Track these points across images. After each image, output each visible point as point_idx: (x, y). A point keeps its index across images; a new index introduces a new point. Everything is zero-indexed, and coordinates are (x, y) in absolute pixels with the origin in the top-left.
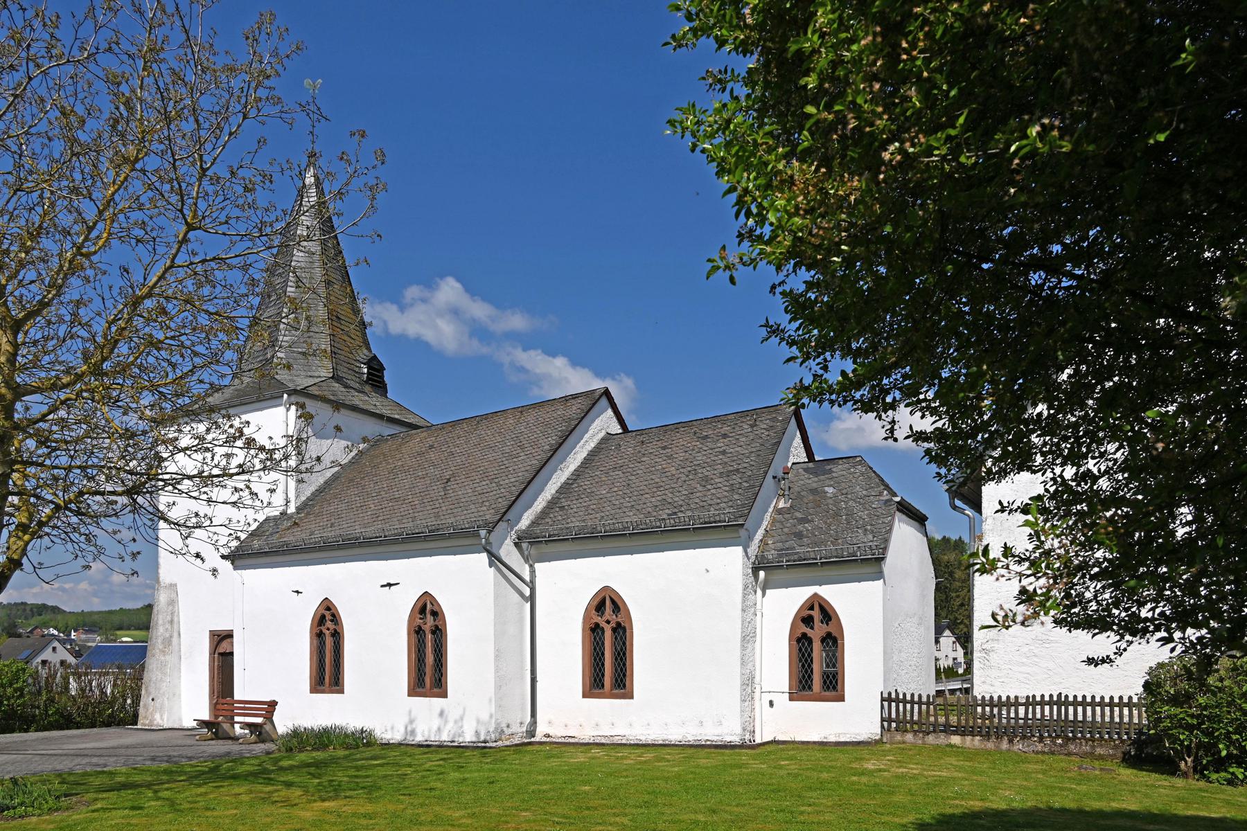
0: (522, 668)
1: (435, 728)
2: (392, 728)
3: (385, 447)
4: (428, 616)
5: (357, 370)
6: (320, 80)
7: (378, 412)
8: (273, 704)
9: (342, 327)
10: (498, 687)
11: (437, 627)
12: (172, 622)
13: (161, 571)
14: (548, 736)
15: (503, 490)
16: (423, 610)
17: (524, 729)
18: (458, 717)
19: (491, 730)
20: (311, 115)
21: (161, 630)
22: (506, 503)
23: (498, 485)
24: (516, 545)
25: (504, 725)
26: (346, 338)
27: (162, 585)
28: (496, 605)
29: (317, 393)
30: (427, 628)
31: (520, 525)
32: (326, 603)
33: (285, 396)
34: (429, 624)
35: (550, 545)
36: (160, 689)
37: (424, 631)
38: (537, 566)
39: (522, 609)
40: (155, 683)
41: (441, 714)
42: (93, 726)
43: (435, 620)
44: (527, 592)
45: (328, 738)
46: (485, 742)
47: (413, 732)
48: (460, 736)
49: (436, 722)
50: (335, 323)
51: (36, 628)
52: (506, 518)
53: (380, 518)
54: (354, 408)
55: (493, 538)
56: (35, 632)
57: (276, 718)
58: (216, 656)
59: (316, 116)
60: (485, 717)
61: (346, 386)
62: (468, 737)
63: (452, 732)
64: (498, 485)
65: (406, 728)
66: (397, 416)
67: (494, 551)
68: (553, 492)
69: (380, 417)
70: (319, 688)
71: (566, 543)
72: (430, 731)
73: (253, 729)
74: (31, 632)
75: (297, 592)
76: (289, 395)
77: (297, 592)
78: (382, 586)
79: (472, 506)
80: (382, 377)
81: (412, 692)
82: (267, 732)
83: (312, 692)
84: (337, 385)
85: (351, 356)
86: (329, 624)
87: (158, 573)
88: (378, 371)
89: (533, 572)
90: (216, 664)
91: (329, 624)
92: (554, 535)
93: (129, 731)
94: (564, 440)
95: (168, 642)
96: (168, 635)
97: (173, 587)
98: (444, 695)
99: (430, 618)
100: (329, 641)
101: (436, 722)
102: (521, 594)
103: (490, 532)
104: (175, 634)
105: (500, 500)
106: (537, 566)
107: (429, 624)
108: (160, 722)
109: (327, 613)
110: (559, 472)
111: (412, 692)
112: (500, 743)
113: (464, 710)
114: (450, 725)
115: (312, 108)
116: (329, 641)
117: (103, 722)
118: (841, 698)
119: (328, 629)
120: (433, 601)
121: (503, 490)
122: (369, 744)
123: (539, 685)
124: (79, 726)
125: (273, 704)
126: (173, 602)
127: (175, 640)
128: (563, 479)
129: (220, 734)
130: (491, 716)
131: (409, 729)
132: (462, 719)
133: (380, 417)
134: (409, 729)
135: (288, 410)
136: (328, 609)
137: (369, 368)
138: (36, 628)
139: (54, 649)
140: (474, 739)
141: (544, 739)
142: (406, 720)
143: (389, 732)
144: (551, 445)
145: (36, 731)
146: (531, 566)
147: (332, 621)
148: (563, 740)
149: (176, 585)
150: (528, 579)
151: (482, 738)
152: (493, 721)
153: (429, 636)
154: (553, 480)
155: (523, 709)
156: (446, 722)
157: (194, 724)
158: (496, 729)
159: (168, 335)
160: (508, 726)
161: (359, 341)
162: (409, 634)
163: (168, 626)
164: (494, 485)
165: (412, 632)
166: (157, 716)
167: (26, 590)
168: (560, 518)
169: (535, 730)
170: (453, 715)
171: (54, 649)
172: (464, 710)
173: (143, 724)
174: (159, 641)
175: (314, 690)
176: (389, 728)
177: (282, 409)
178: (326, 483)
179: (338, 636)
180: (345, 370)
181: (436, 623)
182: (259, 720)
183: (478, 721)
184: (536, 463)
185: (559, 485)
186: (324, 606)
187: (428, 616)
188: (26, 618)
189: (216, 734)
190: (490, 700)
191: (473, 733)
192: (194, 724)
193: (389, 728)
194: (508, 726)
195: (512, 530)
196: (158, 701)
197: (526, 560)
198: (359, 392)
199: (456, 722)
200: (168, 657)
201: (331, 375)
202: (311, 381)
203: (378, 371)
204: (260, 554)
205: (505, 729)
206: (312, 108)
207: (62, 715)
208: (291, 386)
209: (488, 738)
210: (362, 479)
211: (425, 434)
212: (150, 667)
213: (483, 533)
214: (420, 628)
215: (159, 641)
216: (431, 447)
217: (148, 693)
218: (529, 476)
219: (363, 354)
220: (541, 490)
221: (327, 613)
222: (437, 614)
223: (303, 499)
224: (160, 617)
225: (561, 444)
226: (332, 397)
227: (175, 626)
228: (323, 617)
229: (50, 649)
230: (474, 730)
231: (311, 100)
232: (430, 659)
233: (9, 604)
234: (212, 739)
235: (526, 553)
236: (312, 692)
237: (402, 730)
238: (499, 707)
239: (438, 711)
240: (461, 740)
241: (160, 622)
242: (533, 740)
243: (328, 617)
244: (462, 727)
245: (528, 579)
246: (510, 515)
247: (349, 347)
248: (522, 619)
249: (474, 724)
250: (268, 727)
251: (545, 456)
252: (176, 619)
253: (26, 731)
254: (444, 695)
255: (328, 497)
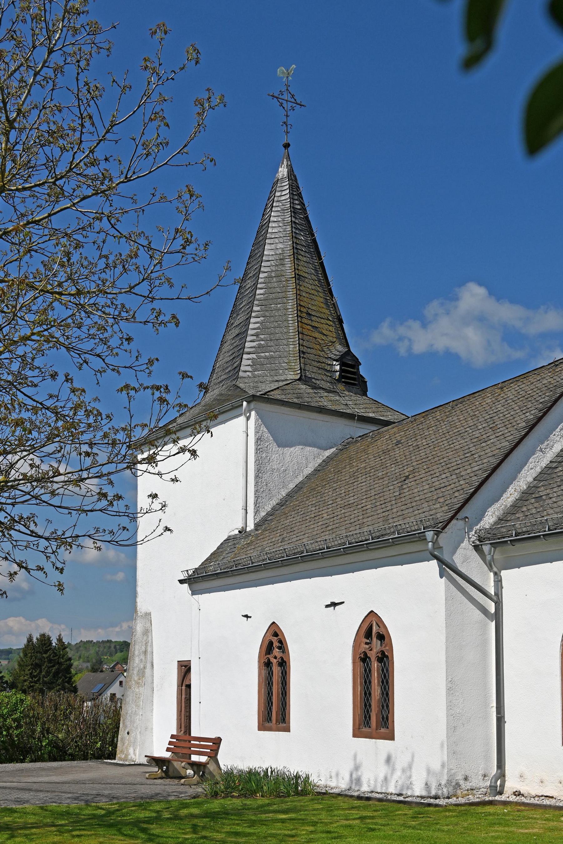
0: (486, 705)
1: (381, 777)
2: (337, 775)
3: (352, 449)
4: (374, 639)
5: (328, 368)
6: (294, 66)
7: (348, 411)
8: (217, 742)
9: (314, 324)
10: (452, 729)
11: (383, 653)
12: (145, 652)
13: (139, 600)
14: (518, 794)
15: (462, 482)
16: (368, 634)
17: (488, 784)
18: (406, 765)
19: (443, 782)
20: (285, 105)
21: (137, 660)
22: (462, 497)
23: (459, 476)
24: (477, 548)
25: (459, 777)
26: (317, 335)
27: (139, 614)
28: (448, 626)
29: (279, 397)
30: (373, 655)
31: (482, 523)
32: (273, 628)
33: (245, 403)
34: (375, 650)
35: (518, 545)
36: (134, 722)
37: (369, 658)
38: (504, 573)
39: (485, 628)
40: (131, 716)
41: (388, 760)
42: (85, 758)
43: (381, 645)
44: (492, 607)
45: (258, 782)
46: (436, 797)
47: (358, 781)
48: (408, 788)
49: (383, 770)
50: (304, 321)
51: (117, 663)
52: (461, 515)
53: (330, 528)
54: (321, 410)
55: (443, 539)
56: (117, 668)
57: (220, 757)
58: (184, 688)
59: (290, 104)
60: (436, 766)
61: (315, 387)
62: (418, 790)
63: (400, 783)
64: (459, 476)
65: (351, 775)
66: (371, 415)
67: (446, 557)
68: (530, 479)
69: (351, 417)
70: (267, 725)
71: (537, 542)
72: (376, 781)
73: (195, 768)
74: (114, 667)
75: (247, 616)
76: (249, 402)
77: (247, 616)
78: (327, 606)
79: (425, 505)
80: (357, 373)
81: (357, 734)
82: (211, 773)
83: (260, 729)
84: (304, 387)
85: (321, 354)
86: (276, 652)
87: (135, 602)
88: (352, 366)
89: (498, 582)
90: (183, 696)
91: (276, 652)
92: (524, 533)
93: (105, 765)
94: (545, 414)
95: (142, 673)
96: (142, 666)
97: (148, 615)
98: (391, 737)
99: (375, 642)
100: (276, 669)
101: (383, 770)
102: (484, 611)
103: (437, 533)
104: (149, 666)
105: (457, 494)
106: (504, 573)
107: (375, 650)
108: (133, 757)
109: (275, 639)
110: (539, 454)
111: (357, 734)
112: (453, 800)
113: (413, 757)
114: (398, 773)
115: (286, 96)
116: (276, 669)
117: (93, 755)
118: (288, 730)
119: (275, 658)
120: (380, 622)
121: (462, 482)
122: (304, 793)
123: (508, 728)
124: (73, 758)
125: (217, 742)
126: (147, 632)
127: (148, 671)
128: (544, 462)
129: (171, 773)
130: (443, 766)
131: (354, 776)
132: (410, 767)
133: (351, 417)
134: (354, 776)
135: (248, 418)
136: (276, 635)
137: (342, 364)
138: (117, 663)
139: (121, 683)
140: (424, 793)
141: (513, 798)
142: (350, 766)
143: (334, 779)
144: (527, 421)
145: (31, 762)
146: (495, 574)
147: (280, 648)
148: (536, 801)
149: (150, 614)
150: (492, 591)
151: (433, 793)
152: (446, 771)
153: (375, 665)
154: (530, 464)
155: (487, 758)
156: (393, 770)
157: (144, 761)
158: (449, 782)
159: (35, 331)
160: (466, 779)
161: (332, 336)
162: (354, 662)
163: (142, 657)
164: (454, 477)
165: (358, 660)
166: (131, 751)
167: (111, 629)
168: (534, 511)
169: (503, 785)
170: (401, 762)
171: (121, 683)
172: (413, 757)
173: (120, 759)
174: (135, 672)
175: (262, 727)
176: (333, 774)
177: (242, 419)
178: (288, 495)
179: (284, 664)
180: (315, 370)
181: (383, 649)
182: (203, 759)
183: (429, 771)
184: (506, 445)
185: (538, 470)
186: (271, 631)
187: (374, 639)
188: (111, 655)
189: (166, 772)
190: (442, 746)
191: (423, 785)
192: (144, 761)
193: (333, 774)
194: (466, 779)
195: (471, 529)
196: (132, 734)
197: (491, 569)
198: (329, 391)
199: (404, 771)
200: (141, 689)
201: (298, 377)
202: (274, 386)
203: (352, 366)
204: (217, 576)
205: (462, 782)
206: (286, 96)
207: (57, 747)
208: (251, 392)
209: (440, 793)
210: (323, 486)
211: (395, 430)
212: (127, 700)
213: (430, 535)
214: (365, 654)
215: (135, 672)
216: (399, 442)
217: (125, 727)
218: (494, 461)
219: (340, 349)
220: (513, 478)
221: (275, 639)
222: (383, 637)
223: (263, 514)
224: (137, 647)
225: (540, 419)
226: (296, 400)
227: (149, 656)
228: (271, 644)
229: (118, 683)
230: (424, 782)
231: (284, 89)
232: (376, 691)
233: (98, 642)
234: (161, 778)
235: (488, 558)
236: (260, 729)
237: (347, 778)
238: (453, 753)
239: (384, 757)
240: (409, 793)
241: (137, 653)
242: (498, 798)
243: (276, 644)
244: (410, 777)
245: (492, 591)
246: (467, 512)
247: (320, 344)
248: (485, 643)
249: (424, 774)
250: (212, 767)
251: (518, 436)
252: (149, 649)
253: (22, 761)
254: (391, 737)
255: (286, 511)
